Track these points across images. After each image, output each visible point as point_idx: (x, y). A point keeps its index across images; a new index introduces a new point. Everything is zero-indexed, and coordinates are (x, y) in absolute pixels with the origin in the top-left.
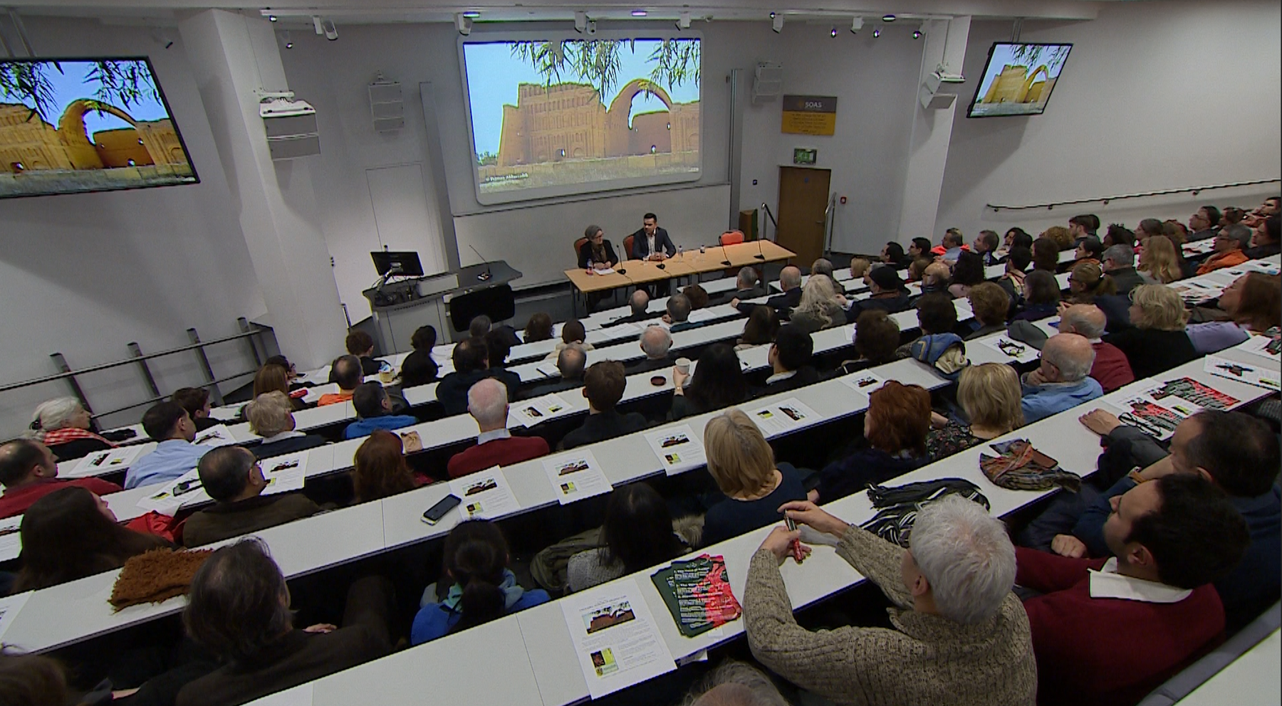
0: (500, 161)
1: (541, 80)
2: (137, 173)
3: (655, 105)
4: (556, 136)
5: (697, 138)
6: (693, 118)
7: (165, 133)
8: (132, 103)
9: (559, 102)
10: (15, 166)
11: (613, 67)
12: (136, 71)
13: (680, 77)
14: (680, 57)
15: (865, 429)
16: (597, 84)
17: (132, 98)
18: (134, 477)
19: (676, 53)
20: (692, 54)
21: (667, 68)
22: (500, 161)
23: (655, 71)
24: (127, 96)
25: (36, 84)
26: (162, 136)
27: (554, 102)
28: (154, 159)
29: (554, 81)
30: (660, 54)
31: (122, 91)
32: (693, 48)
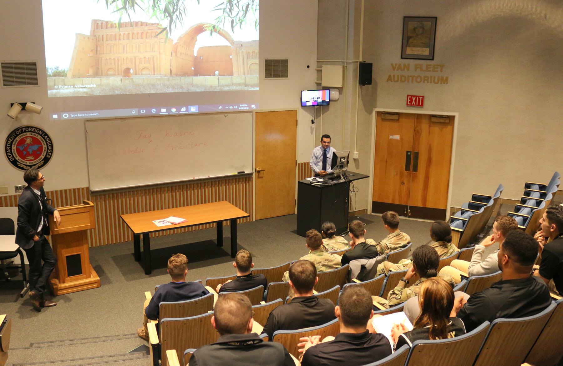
0: (69, 75)
1: (114, 18)
2: (217, 80)
3: (218, 41)
4: (125, 58)
5: (257, 67)
6: (253, 52)
7: (251, 52)
8: (237, 28)
9: (128, 34)
10: (127, 72)
11: (180, 13)
12: (250, 6)
13: (241, 23)
14: (241, 9)
15: (26, 273)
16: (165, 23)
17: (239, 24)
18: (468, 305)
19: (238, 7)
20: (252, 8)
21: (229, 16)
22: (69, 75)
23: (219, 17)
24: (236, 22)
25: (177, 10)
26: (248, 54)
27: (124, 34)
28: (235, 71)
29: (125, 19)
30: (223, 6)
31: (234, 19)
32: (253, 5)
